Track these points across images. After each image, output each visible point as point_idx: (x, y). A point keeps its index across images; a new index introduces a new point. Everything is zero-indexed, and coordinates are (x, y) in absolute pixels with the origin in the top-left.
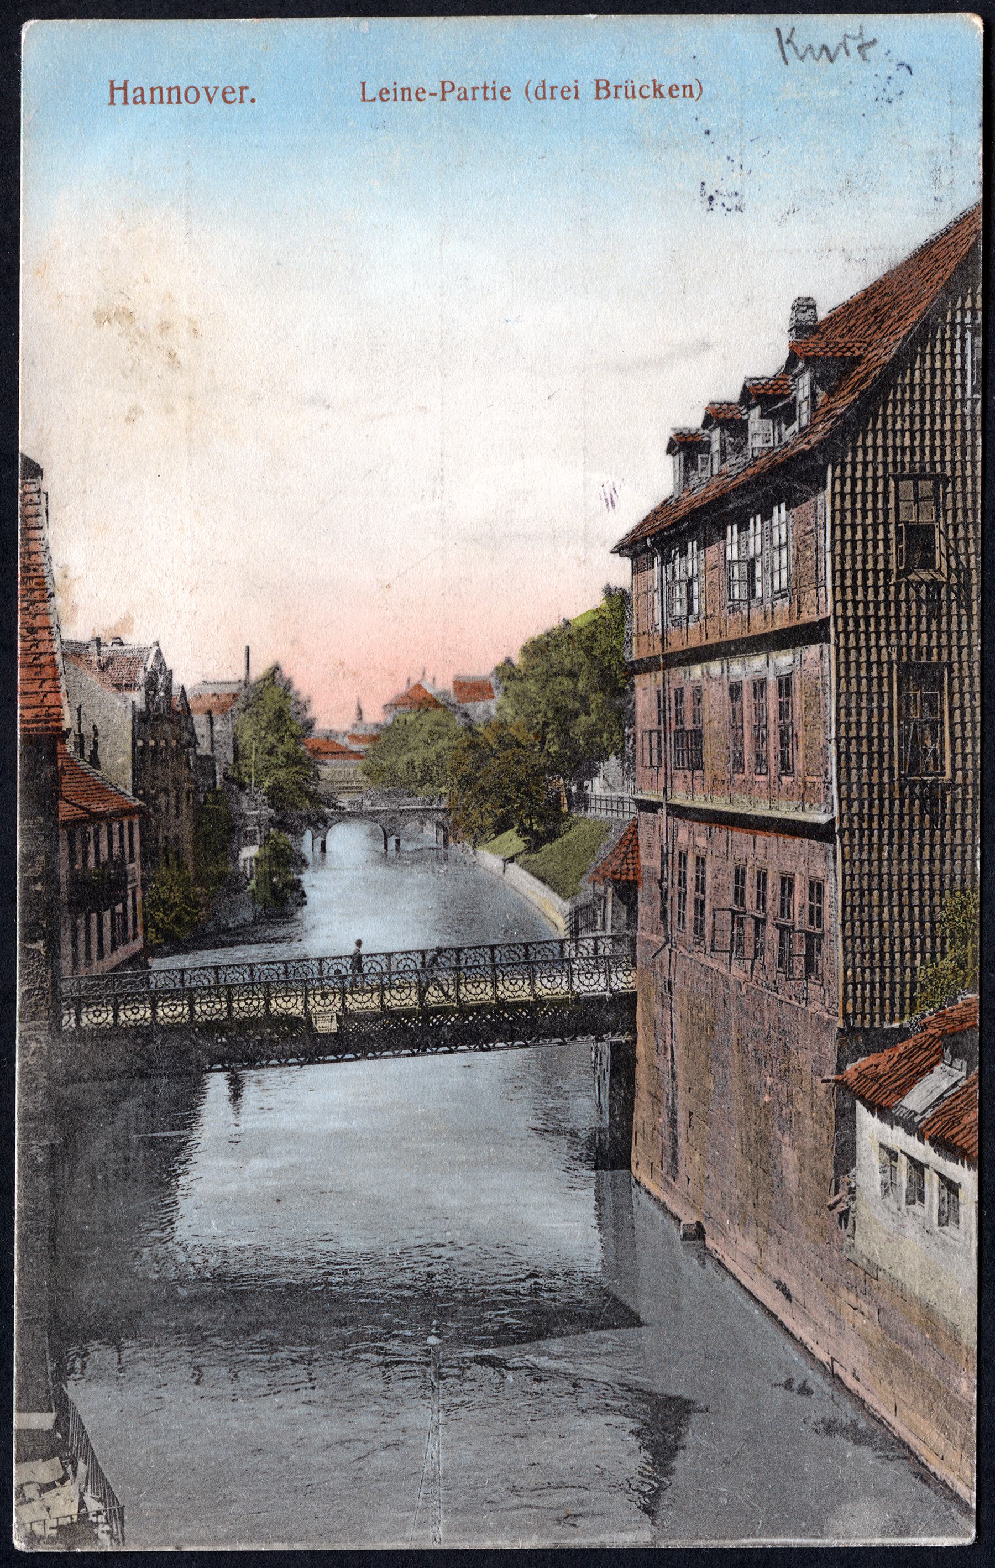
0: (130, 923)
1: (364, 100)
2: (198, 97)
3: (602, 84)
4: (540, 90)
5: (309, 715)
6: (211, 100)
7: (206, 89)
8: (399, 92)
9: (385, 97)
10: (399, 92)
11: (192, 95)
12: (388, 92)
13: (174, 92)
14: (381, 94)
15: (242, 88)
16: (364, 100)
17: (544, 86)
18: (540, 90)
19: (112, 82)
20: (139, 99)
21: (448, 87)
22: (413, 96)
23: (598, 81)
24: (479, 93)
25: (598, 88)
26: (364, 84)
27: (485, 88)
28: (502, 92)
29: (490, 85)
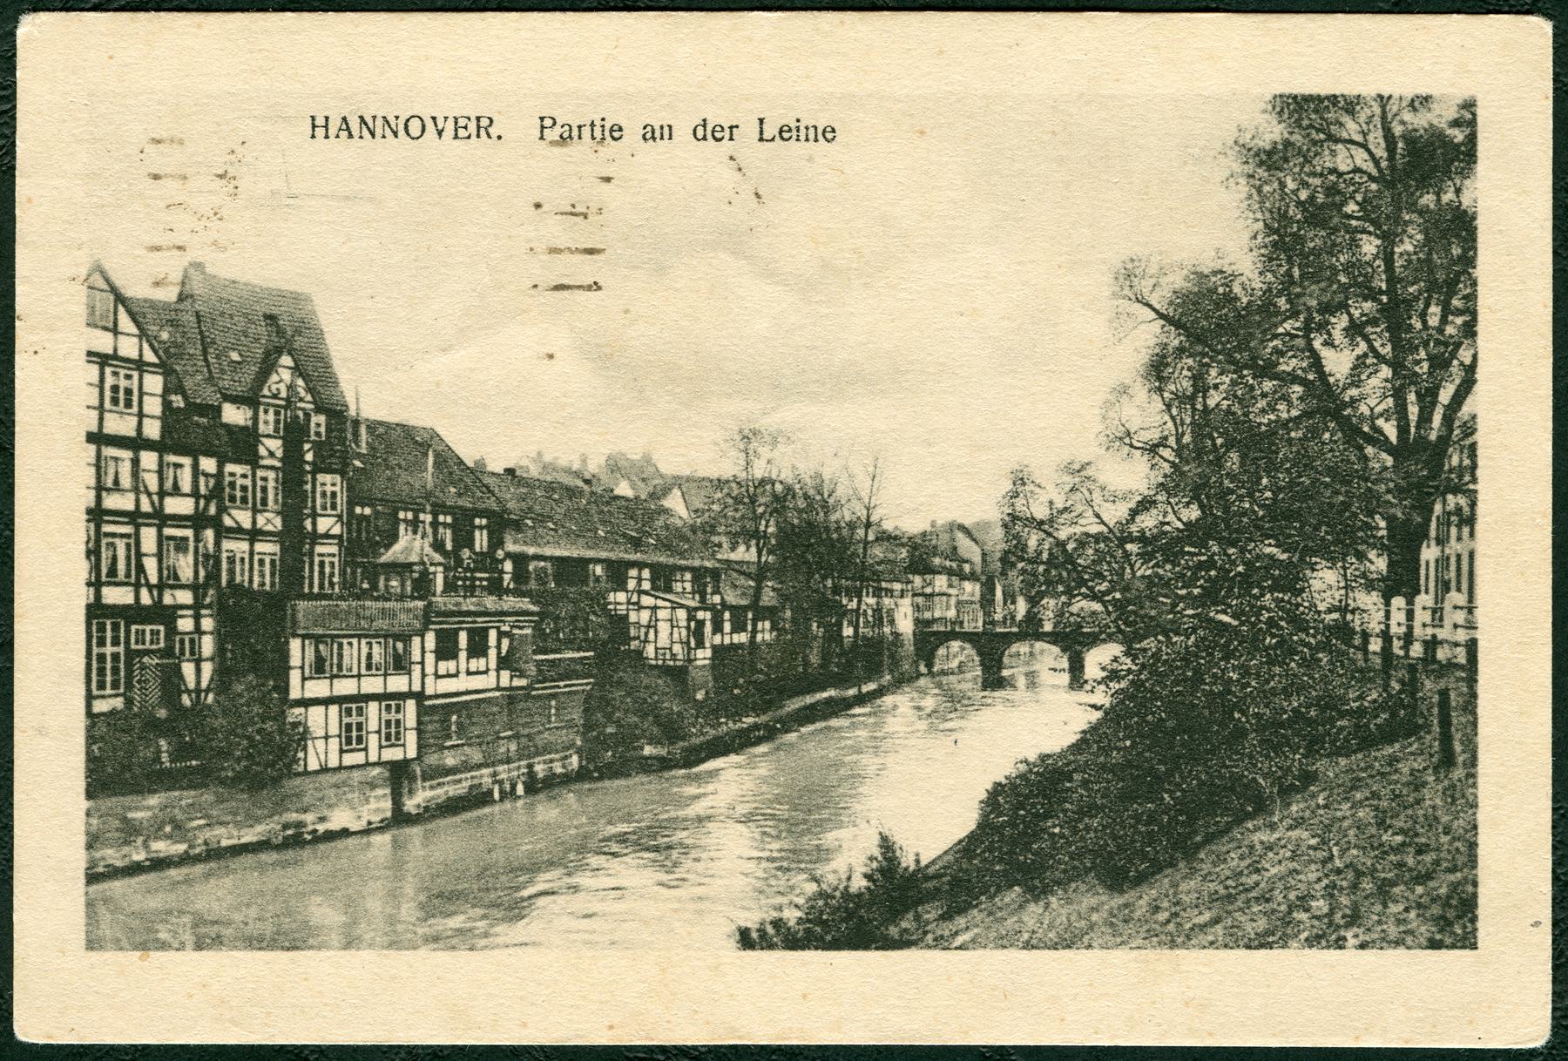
0: (94, 672)
1: (761, 139)
2: (423, 131)
3: (320, 121)
4: (700, 129)
5: (869, 762)
6: (440, 133)
7: (434, 118)
8: (803, 131)
9: (786, 135)
10: (803, 131)
11: (415, 127)
12: (790, 130)
13: (812, 131)
14: (781, 131)
15: (731, 128)
16: (761, 139)
17: (704, 126)
18: (700, 129)
19: (313, 118)
20: (649, 136)
21: (548, 122)
22: (820, 137)
23: (542, 119)
24: (586, 132)
25: (314, 126)
26: (761, 121)
27: (593, 125)
28: (612, 130)
29: (598, 123)
